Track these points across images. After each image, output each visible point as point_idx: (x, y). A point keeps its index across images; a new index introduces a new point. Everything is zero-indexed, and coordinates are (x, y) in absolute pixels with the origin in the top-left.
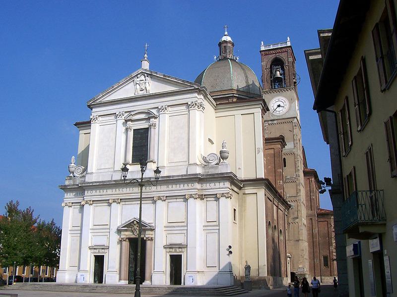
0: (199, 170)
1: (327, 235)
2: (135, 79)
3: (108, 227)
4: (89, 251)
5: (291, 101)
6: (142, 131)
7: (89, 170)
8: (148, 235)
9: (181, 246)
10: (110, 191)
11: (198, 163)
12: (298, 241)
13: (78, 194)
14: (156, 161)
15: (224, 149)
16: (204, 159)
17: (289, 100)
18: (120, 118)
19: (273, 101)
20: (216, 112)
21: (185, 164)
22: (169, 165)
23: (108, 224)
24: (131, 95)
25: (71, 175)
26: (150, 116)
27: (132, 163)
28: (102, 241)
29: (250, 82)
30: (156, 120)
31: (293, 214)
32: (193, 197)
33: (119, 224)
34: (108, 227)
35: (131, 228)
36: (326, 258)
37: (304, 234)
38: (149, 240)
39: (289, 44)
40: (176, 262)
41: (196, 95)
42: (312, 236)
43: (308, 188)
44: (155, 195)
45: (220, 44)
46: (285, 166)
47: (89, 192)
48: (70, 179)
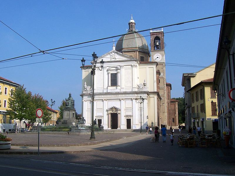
0: (136, 90)
2: (111, 54)
5: (163, 56)
8: (119, 112)
9: (130, 116)
10: (103, 96)
11: (136, 87)
12: (164, 112)
14: (120, 86)
15: (145, 83)
16: (138, 86)
19: (155, 55)
25: (85, 89)
26: (117, 69)
28: (101, 114)
31: (162, 102)
33: (107, 108)
36: (173, 119)
37: (166, 110)
39: (162, 31)
40: (129, 122)
41: (134, 62)
42: (169, 110)
44: (121, 98)
45: (129, 24)
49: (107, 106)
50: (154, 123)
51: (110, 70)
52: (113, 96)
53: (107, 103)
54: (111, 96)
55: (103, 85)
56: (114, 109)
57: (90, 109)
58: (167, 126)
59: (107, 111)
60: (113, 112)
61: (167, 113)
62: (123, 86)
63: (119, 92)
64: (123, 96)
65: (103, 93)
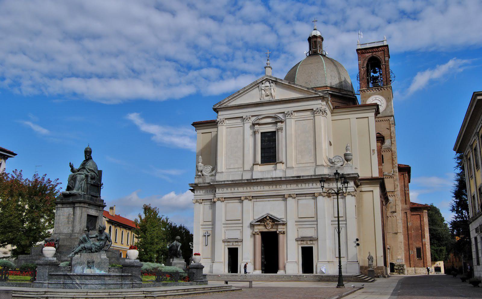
0: (325, 171)
1: (420, 228)
2: (260, 85)
3: (240, 222)
4: (223, 244)
6: (269, 134)
7: (219, 170)
8: (280, 229)
9: (311, 239)
10: (241, 189)
11: (325, 164)
12: (396, 233)
13: (208, 191)
14: (284, 161)
15: (348, 152)
17: (385, 98)
18: (247, 122)
20: (332, 116)
21: (311, 165)
24: (257, 100)
25: (200, 174)
26: (277, 121)
27: (261, 163)
28: (236, 235)
29: (343, 79)
30: (282, 124)
31: (392, 208)
34: (240, 222)
35: (264, 222)
36: (419, 251)
37: (401, 229)
38: (281, 233)
43: (403, 183)
44: (286, 193)
46: (383, 163)
47: (220, 190)
48: (199, 178)
50: (374, 258)
51: (259, 124)
52: (266, 188)
54: (262, 187)
55: (240, 162)
56: (268, 222)
58: (405, 267)
59: (252, 226)
61: (402, 236)
62: (292, 162)
63: (281, 178)
64: (293, 189)
65: (242, 180)
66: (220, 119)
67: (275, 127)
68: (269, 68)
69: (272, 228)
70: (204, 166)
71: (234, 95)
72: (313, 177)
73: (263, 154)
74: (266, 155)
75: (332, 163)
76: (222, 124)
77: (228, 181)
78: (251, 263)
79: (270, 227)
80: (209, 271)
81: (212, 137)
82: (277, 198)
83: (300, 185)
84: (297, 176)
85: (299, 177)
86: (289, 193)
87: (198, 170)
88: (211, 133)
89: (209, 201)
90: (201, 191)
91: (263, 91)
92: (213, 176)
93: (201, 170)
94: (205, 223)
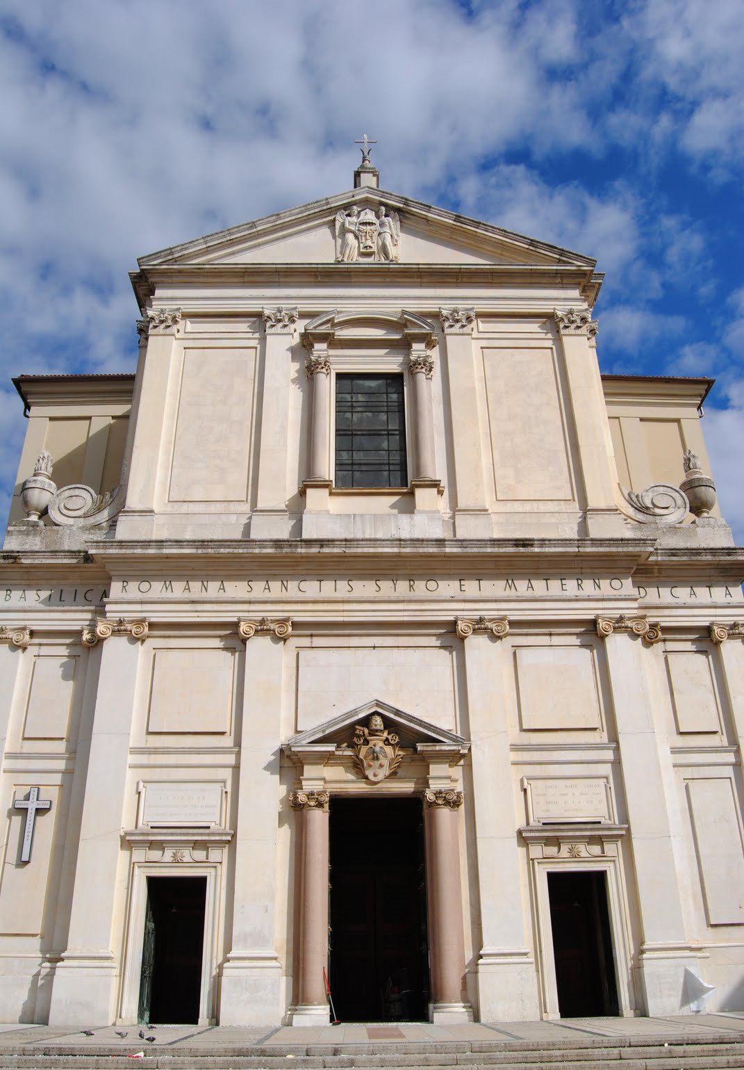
2: (340, 218)
4: (123, 856)
8: (442, 778)
21: (563, 507)
22: (169, 509)
23: (226, 725)
32: (127, 633)
33: (284, 735)
35: (352, 745)
38: (448, 803)
44: (464, 613)
49: (286, 712)
52: (365, 588)
53: (286, 675)
54: (342, 585)
56: (377, 743)
57: (61, 747)
60: (356, 787)
65: (246, 541)
66: (162, 311)
67: (400, 359)
68: (374, 175)
69: (393, 775)
70: (58, 489)
71: (231, 234)
72: (589, 550)
73: (345, 455)
74: (359, 457)
75: (643, 509)
76: (168, 331)
77: (179, 543)
78: (273, 963)
79: (386, 771)
80: (24, 1012)
81: (90, 435)
82: (415, 638)
83: (522, 585)
84: (517, 540)
85: (524, 546)
86: (730, 621)
87: (26, 503)
88: (88, 422)
89: (68, 641)
90: (31, 594)
91: (350, 237)
92: (99, 529)
93: (43, 506)
94: (30, 747)
